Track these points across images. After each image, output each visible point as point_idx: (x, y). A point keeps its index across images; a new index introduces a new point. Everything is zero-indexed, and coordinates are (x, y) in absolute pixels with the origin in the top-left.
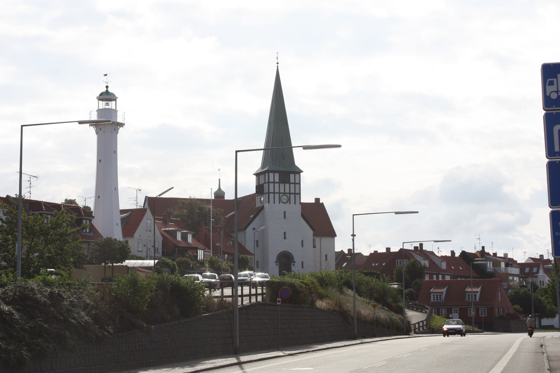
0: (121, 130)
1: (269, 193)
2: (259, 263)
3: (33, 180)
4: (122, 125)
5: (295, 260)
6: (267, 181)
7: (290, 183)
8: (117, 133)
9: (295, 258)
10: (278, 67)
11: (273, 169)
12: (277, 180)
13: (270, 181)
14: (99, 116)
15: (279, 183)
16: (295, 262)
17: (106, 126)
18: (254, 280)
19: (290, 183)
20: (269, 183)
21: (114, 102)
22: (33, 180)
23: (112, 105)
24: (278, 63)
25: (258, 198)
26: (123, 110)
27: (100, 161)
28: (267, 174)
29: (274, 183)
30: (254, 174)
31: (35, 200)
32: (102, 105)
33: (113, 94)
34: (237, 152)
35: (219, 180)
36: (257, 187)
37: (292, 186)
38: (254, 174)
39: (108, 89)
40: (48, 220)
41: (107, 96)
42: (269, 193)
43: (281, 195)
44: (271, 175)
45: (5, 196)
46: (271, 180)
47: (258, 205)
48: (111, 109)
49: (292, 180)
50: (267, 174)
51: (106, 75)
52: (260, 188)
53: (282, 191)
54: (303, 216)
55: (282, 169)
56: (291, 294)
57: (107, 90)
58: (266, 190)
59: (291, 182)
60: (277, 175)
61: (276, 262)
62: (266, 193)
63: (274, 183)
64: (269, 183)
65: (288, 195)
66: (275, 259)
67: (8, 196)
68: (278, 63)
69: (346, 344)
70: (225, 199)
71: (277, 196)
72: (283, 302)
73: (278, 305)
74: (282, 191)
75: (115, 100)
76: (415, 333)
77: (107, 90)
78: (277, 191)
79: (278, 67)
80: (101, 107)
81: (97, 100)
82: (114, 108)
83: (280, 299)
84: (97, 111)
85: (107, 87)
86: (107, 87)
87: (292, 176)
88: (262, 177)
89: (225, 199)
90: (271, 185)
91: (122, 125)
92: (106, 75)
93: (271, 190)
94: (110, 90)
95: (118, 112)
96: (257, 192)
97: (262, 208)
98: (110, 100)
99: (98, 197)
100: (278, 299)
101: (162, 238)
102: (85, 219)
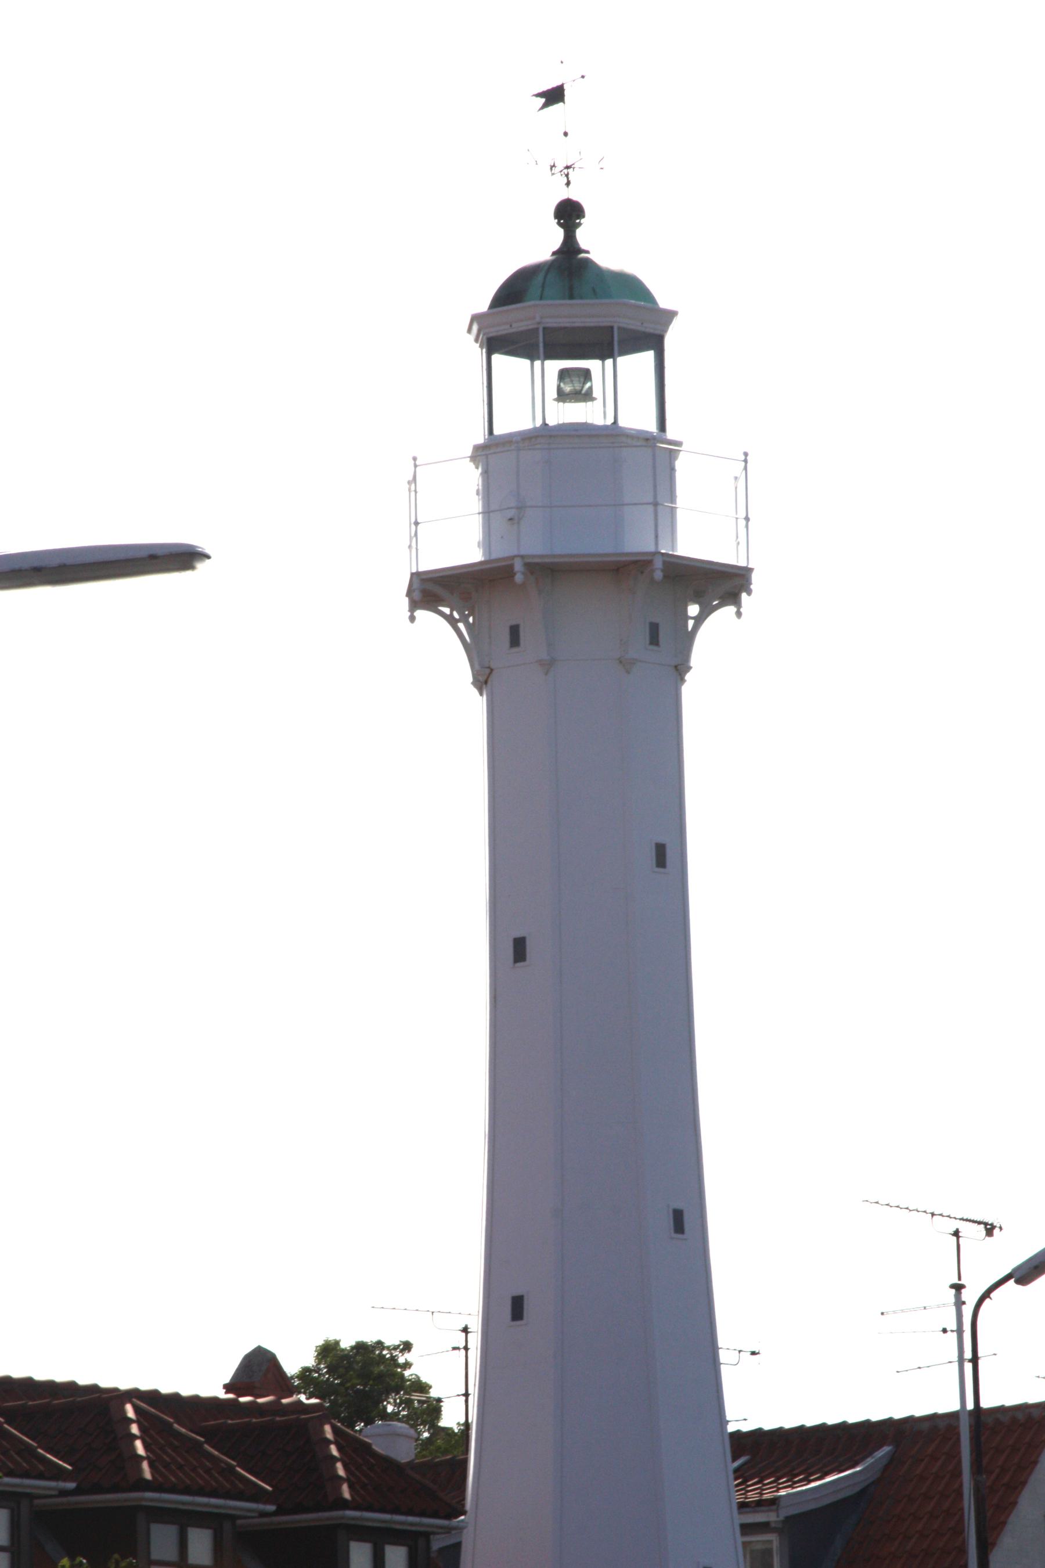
0: (717, 638)
4: (725, 584)
8: (680, 669)
14: (501, 504)
17: (579, 607)
18: (765, 1497)
21: (648, 357)
23: (622, 391)
26: (732, 447)
27: (520, 950)
31: (60, 1376)
32: (526, 393)
33: (630, 287)
39: (583, 237)
40: (926, 1426)
41: (567, 306)
48: (612, 436)
51: (554, 96)
57: (569, 249)
75: (655, 342)
77: (569, 249)
80: (515, 418)
81: (476, 353)
82: (638, 417)
84: (483, 454)
85: (569, 214)
86: (569, 214)
91: (725, 584)
92: (554, 96)
94: (602, 245)
95: (681, 464)
98: (605, 344)
99: (508, 1307)
102: (362, 1533)
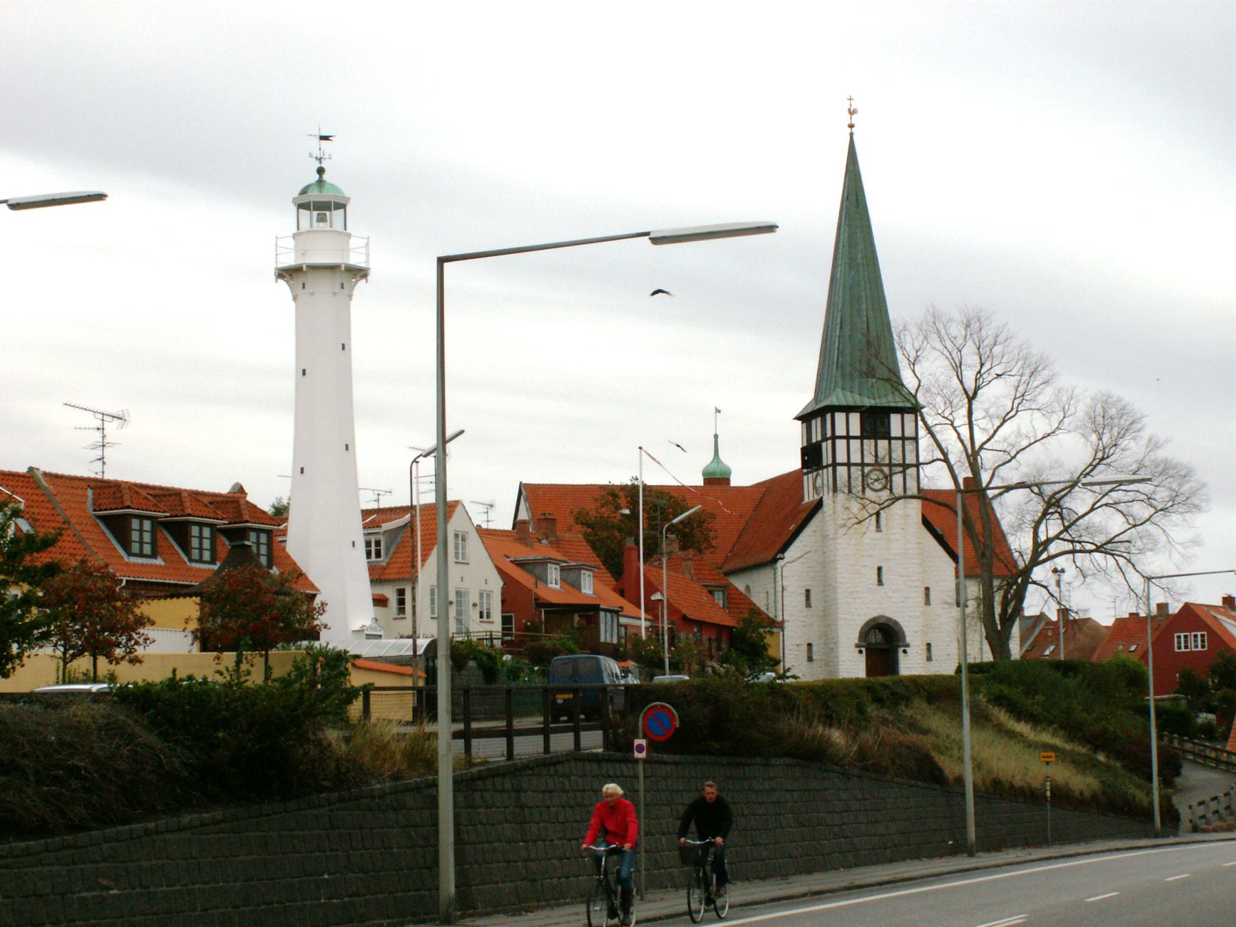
1: (835, 465)
2: (814, 648)
3: (111, 427)
5: (908, 640)
6: (829, 434)
7: (890, 438)
9: (907, 634)
10: (851, 134)
11: (844, 403)
12: (855, 430)
13: (837, 433)
15: (861, 438)
16: (908, 646)
19: (890, 438)
20: (834, 438)
22: (111, 427)
24: (851, 126)
25: (808, 481)
28: (828, 416)
29: (848, 437)
30: (798, 418)
34: (442, 261)
35: (716, 436)
36: (804, 451)
37: (897, 445)
38: (798, 418)
42: (835, 465)
43: (867, 469)
44: (840, 417)
45: (23, 470)
46: (840, 430)
47: (809, 497)
49: (895, 430)
50: (828, 416)
52: (812, 456)
53: (869, 459)
54: (926, 523)
55: (868, 402)
56: (677, 724)
58: (827, 459)
59: (893, 434)
60: (855, 418)
61: (857, 646)
62: (827, 466)
63: (848, 437)
64: (834, 438)
65: (886, 469)
66: (854, 637)
67: (31, 469)
68: (851, 126)
69: (757, 897)
70: (732, 484)
71: (856, 472)
72: (653, 746)
73: (637, 761)
74: (869, 459)
76: (1195, 829)
78: (856, 458)
79: (851, 134)
83: (643, 742)
85: (321, 171)
86: (321, 171)
87: (895, 419)
88: (816, 424)
89: (732, 484)
90: (841, 445)
93: (841, 457)
96: (805, 464)
97: (819, 505)
100: (637, 742)
101: (501, 583)
